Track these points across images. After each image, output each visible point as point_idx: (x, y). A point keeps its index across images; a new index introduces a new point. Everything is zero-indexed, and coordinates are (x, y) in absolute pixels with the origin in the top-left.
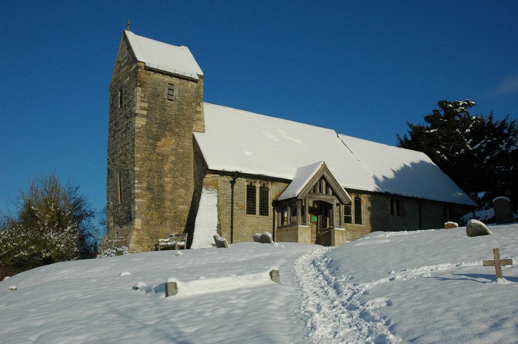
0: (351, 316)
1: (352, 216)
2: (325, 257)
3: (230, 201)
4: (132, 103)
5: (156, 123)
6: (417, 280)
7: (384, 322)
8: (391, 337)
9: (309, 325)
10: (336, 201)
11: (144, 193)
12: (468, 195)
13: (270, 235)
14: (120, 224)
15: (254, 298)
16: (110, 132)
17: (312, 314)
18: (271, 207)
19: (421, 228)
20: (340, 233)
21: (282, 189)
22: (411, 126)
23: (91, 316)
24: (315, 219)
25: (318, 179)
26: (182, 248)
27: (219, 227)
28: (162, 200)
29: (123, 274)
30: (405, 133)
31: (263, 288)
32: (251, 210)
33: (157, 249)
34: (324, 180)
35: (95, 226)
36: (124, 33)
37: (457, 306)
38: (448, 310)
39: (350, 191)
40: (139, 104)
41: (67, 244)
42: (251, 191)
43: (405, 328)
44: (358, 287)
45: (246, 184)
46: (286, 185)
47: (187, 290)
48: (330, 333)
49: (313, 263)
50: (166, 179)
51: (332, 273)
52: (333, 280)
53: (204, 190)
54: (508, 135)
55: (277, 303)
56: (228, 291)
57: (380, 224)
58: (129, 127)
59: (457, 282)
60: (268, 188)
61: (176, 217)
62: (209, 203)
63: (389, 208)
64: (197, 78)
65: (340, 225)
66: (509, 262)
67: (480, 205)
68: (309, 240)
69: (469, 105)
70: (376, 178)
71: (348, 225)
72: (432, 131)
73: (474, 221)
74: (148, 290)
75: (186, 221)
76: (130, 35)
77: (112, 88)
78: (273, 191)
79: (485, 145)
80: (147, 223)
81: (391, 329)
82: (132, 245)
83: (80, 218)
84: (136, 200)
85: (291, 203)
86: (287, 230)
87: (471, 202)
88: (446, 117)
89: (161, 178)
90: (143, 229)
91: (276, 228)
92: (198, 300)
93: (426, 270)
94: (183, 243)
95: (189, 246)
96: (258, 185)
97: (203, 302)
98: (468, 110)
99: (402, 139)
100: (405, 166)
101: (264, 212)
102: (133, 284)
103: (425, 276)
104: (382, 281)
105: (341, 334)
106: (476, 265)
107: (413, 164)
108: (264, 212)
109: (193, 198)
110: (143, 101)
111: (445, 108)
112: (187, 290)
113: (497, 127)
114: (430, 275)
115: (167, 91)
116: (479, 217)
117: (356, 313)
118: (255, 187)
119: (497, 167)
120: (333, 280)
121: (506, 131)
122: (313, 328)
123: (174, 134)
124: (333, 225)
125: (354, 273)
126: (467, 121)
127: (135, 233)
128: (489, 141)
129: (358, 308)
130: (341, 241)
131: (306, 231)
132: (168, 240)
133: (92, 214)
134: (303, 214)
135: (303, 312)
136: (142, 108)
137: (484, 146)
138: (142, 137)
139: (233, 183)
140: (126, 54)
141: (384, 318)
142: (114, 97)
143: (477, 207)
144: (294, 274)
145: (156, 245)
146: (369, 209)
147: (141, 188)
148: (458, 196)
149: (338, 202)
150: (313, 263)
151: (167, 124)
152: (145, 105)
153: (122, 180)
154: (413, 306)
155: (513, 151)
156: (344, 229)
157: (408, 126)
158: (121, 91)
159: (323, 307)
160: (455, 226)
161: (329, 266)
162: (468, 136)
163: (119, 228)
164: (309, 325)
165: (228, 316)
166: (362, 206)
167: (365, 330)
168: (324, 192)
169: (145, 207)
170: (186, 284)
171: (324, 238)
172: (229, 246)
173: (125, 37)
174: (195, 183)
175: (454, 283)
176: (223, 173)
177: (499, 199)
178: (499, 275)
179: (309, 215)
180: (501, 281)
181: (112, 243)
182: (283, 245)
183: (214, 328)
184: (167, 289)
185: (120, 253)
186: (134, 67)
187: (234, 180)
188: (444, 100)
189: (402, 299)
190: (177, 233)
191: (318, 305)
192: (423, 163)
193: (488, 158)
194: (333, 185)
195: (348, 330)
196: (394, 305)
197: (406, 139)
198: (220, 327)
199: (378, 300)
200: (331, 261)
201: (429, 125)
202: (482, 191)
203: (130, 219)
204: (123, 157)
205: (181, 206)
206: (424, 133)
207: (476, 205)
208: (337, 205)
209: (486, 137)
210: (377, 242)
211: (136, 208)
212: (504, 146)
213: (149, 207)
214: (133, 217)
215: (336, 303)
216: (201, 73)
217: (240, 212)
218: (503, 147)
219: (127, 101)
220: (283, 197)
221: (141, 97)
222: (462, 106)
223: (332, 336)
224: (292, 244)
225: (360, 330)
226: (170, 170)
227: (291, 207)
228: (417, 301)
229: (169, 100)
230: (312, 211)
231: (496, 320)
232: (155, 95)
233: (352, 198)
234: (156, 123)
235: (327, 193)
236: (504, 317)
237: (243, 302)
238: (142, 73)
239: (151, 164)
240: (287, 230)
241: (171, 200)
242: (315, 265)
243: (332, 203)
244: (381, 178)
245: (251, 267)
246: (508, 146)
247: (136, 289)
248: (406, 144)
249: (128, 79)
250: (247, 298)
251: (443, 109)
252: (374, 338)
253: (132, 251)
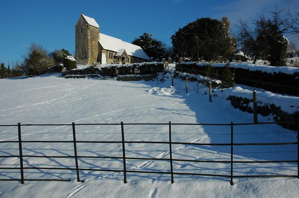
10: (126, 57)
18: (113, 57)
32: (110, 58)
40: (89, 33)
42: (110, 53)
54: (160, 44)
61: (95, 58)
87: (150, 60)
88: (145, 38)
89: (93, 50)
96: (111, 53)
101: (112, 58)
111: (145, 35)
119: (164, 55)
123: (95, 40)
126: (151, 39)
139: (107, 52)
140: (83, 20)
162: (151, 44)
173: (84, 19)
213: (91, 56)
232: (91, 31)
246: (159, 47)
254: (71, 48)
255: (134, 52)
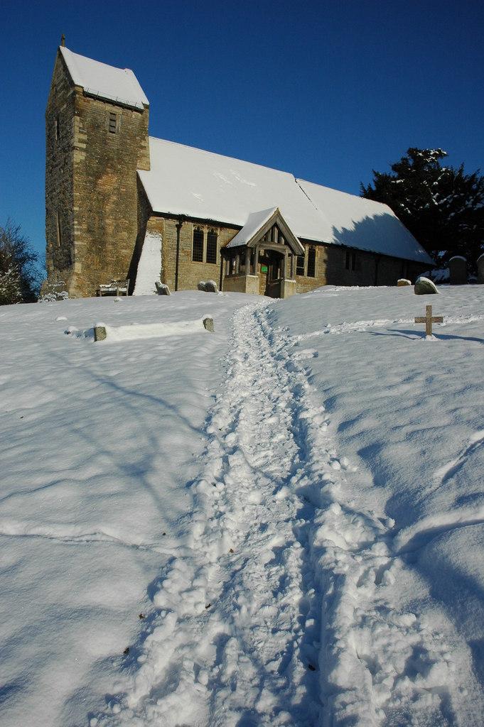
0: (276, 366)
1: (305, 267)
2: (267, 308)
3: (176, 247)
4: (69, 135)
5: (97, 158)
6: (351, 334)
7: (305, 372)
8: (307, 386)
9: (229, 373)
10: (288, 251)
11: (84, 235)
12: (429, 254)
13: (215, 284)
14: (60, 267)
15: (182, 345)
16: (47, 167)
17: (235, 362)
18: (219, 255)
19: (376, 283)
20: (290, 285)
21: (231, 236)
22: (376, 174)
23: (19, 358)
24: (265, 269)
25: (270, 227)
26: (124, 294)
27: (163, 274)
28: (103, 243)
29: (59, 319)
30: (370, 182)
31: (193, 337)
32: (197, 257)
33: (98, 295)
34: (277, 228)
35: (38, 269)
36: (59, 50)
37: (380, 360)
38: (370, 363)
39: (304, 241)
40: (77, 136)
41: (9, 287)
42: (198, 237)
43: (323, 379)
44: (290, 338)
45: (193, 229)
46: (234, 231)
47: (115, 335)
48: (250, 381)
49: (255, 314)
50: (107, 221)
51: (270, 324)
52: (269, 332)
53: (147, 233)
54: (476, 191)
55: (205, 351)
56: (159, 338)
57: (334, 278)
58: (67, 162)
59: (388, 338)
60: (216, 234)
61: (118, 262)
62: (152, 246)
63: (345, 262)
64: (142, 108)
65: (291, 276)
66: (440, 320)
67: (440, 264)
68: (257, 291)
69: (440, 155)
70: (335, 230)
71: (300, 277)
72: (398, 181)
73: (423, 279)
74: (79, 335)
75: (129, 266)
76: (65, 52)
77: (49, 118)
78: (222, 237)
79: (452, 200)
80: (87, 267)
81: (309, 380)
82: (72, 290)
83: (23, 260)
84: (76, 243)
85: (241, 251)
86: (234, 280)
87: (429, 261)
88: (414, 167)
89: (102, 219)
90: (83, 274)
91: (223, 277)
92: (126, 345)
93: (362, 325)
94: (125, 290)
95: (131, 292)
96: (206, 231)
97: (130, 348)
98: (439, 160)
99: (366, 188)
100: (367, 218)
101: (211, 259)
102: (65, 329)
103: (360, 330)
104: (317, 333)
105: (260, 382)
106: (408, 323)
107: (375, 217)
108: (211, 259)
109: (137, 242)
110: (82, 133)
112: (115, 335)
113: (466, 181)
114: (364, 330)
115: (108, 122)
116: (435, 277)
117: (281, 364)
118: (202, 232)
120: (269, 332)
121: (474, 187)
122: (232, 375)
123: (116, 171)
124: (283, 276)
125: (291, 325)
127: (75, 278)
128: (455, 196)
129: (285, 359)
130: (291, 293)
131: (254, 282)
132: (109, 286)
133: (34, 258)
134: (252, 263)
135: (228, 360)
136: (81, 141)
137: (450, 202)
138: (82, 174)
139: (179, 227)
141: (306, 369)
142: (50, 127)
143: (436, 267)
144: (231, 324)
145: (98, 291)
146: (325, 261)
147: (81, 230)
148: (419, 253)
149: (290, 252)
150: (255, 314)
151: (108, 160)
152: (85, 137)
153: (61, 221)
154: (338, 358)
155: (479, 208)
156: (295, 281)
157: (374, 175)
158: (58, 121)
159: (250, 356)
160: (408, 284)
161: (269, 317)
162: (435, 189)
163: (58, 272)
164: (229, 373)
165: (151, 361)
166: (316, 258)
167: (285, 379)
168: (276, 241)
169: (85, 250)
170: (116, 329)
171: (274, 289)
172: (172, 293)
173: (61, 55)
174: (139, 226)
175: (384, 339)
176: (168, 216)
177: (460, 259)
178: (428, 332)
179: (259, 265)
180: (429, 338)
181: (52, 287)
182: (227, 294)
183: (135, 372)
184: (96, 333)
185: (60, 298)
186: (72, 91)
187: (181, 223)
188: (414, 147)
189: (329, 352)
190: (119, 279)
191: (246, 354)
192: (386, 216)
193: (452, 214)
194: (286, 234)
195: (268, 379)
196: (320, 357)
197: (370, 188)
198: (140, 372)
199: (305, 352)
200: (272, 312)
201: (396, 175)
202: (444, 250)
203: (69, 263)
204: (61, 196)
205: (124, 251)
206: (390, 183)
207: (436, 265)
208: (290, 255)
209: (453, 192)
210: (324, 295)
211: (76, 251)
212: (470, 203)
213: (89, 251)
214: (73, 260)
215: (264, 353)
216: (147, 103)
217: (186, 258)
218: (469, 204)
219: (65, 132)
220: (231, 245)
221: (80, 128)
222: (433, 156)
223: (250, 384)
224: (239, 294)
225: (280, 379)
226: (112, 211)
227: (241, 255)
228: (343, 354)
229: (111, 132)
230: (263, 261)
231: (411, 374)
232: (95, 126)
233: (306, 249)
234: (97, 158)
235: (279, 241)
236: (419, 371)
237: (171, 349)
238: (81, 101)
239: (91, 204)
240: (234, 280)
241: (113, 244)
242: (256, 316)
243: (284, 253)
244: (340, 230)
245: (188, 315)
246: (474, 203)
247: (68, 333)
248: (369, 195)
249: (65, 106)
250: (175, 345)
251: (412, 158)
252: (291, 387)
253: (72, 297)
254: (37, 243)
255: (350, 227)
